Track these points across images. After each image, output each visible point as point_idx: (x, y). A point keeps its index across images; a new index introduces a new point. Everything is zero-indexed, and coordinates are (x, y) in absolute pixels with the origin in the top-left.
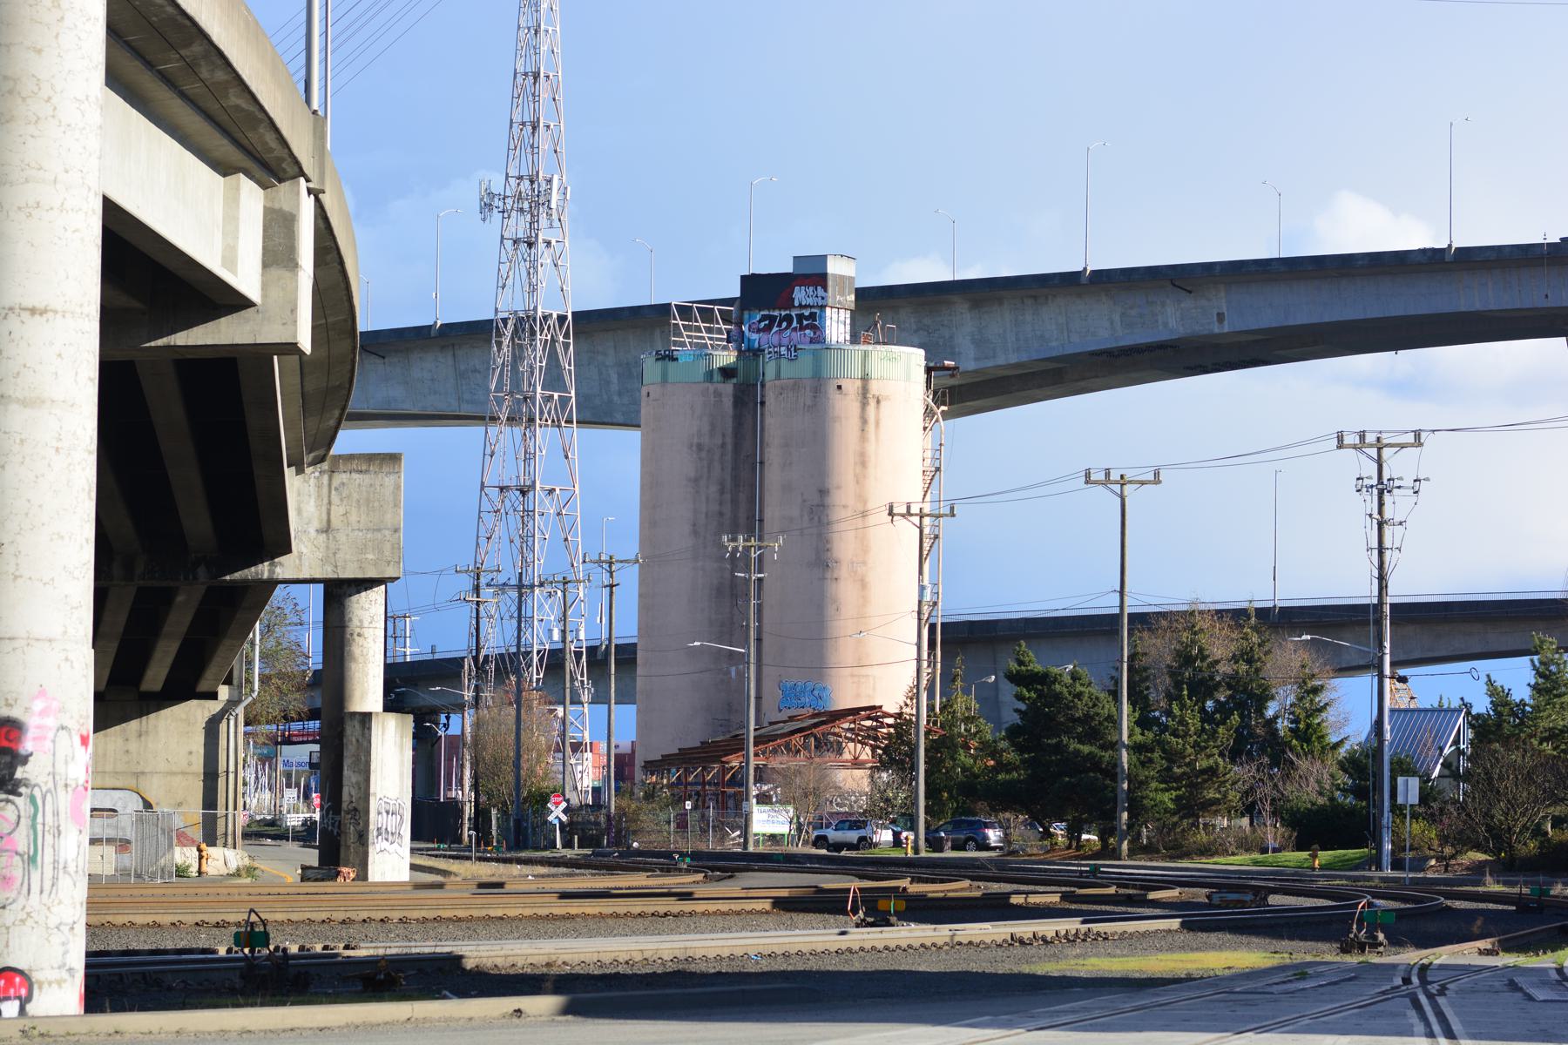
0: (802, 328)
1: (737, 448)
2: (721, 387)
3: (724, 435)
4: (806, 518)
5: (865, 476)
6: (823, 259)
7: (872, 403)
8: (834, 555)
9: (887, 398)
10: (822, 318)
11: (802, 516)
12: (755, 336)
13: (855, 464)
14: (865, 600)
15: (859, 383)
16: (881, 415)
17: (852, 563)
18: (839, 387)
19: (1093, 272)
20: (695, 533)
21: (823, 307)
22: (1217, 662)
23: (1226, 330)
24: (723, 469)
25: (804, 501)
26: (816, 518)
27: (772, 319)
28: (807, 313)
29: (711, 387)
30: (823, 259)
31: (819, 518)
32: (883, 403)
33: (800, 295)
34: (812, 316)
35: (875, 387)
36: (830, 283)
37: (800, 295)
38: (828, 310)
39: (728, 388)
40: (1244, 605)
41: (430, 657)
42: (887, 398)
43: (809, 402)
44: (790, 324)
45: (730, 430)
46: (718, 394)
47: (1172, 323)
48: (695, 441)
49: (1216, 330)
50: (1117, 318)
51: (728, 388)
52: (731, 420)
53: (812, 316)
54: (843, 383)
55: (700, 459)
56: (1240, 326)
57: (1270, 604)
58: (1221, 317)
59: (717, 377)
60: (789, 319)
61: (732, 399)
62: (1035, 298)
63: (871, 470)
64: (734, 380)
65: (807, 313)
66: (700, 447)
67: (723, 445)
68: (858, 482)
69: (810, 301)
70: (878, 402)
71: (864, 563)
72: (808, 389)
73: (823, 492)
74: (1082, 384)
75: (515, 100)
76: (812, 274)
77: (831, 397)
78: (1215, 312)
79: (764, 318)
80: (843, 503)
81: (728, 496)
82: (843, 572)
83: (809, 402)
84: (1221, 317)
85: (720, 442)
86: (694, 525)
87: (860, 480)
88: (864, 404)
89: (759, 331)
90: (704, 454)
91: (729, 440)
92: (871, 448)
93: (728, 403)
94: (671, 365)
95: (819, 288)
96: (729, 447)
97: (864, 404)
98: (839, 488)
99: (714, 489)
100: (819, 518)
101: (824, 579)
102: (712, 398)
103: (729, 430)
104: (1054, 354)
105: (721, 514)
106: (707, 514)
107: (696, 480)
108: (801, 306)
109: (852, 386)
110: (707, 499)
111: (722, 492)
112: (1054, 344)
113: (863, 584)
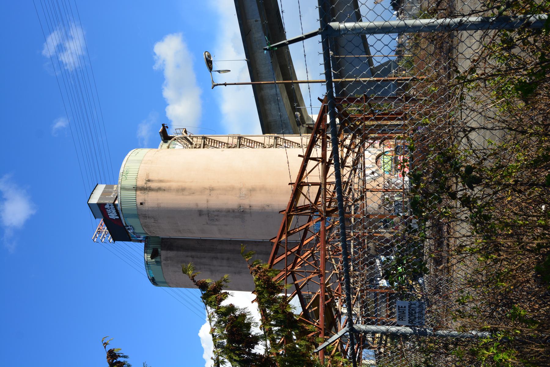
1: (193, 249)
2: (163, 257)
3: (187, 256)
4: (217, 223)
5: (190, 189)
7: (150, 184)
8: (237, 208)
9: (148, 175)
11: (216, 225)
13: (183, 195)
14: (263, 189)
15: (138, 193)
16: (157, 179)
17: (240, 197)
18: (141, 204)
19: (246, 58)
20: (239, 273)
22: (459, 137)
23: (260, 19)
24: (205, 258)
25: (207, 223)
26: (216, 217)
29: (163, 262)
31: (215, 216)
32: (150, 178)
35: (141, 183)
36: (102, 202)
39: (163, 253)
42: (148, 175)
43: (152, 220)
45: (184, 253)
46: (166, 259)
49: (260, 22)
51: (163, 253)
52: (179, 252)
54: (139, 201)
55: (200, 269)
56: (258, 15)
58: (256, 21)
59: (158, 259)
61: (168, 252)
62: (258, 74)
63: (187, 185)
64: (159, 250)
67: (192, 257)
68: (193, 193)
69: (114, 211)
70: (149, 181)
71: (240, 189)
72: (146, 221)
73: (200, 213)
74: (287, 60)
77: (147, 208)
78: (255, 23)
80: (206, 202)
81: (219, 255)
82: (246, 202)
83: (152, 220)
84: (256, 21)
85: (191, 258)
86: (235, 273)
87: (192, 192)
88: (149, 189)
91: (190, 253)
92: (174, 185)
93: (171, 254)
95: (106, 207)
96: (193, 253)
97: (149, 189)
98: (197, 205)
99: (215, 262)
100: (215, 216)
101: (250, 213)
102: (169, 262)
105: (228, 259)
106: (229, 267)
109: (141, 197)
110: (221, 266)
111: (216, 258)
112: (270, 68)
113: (252, 190)
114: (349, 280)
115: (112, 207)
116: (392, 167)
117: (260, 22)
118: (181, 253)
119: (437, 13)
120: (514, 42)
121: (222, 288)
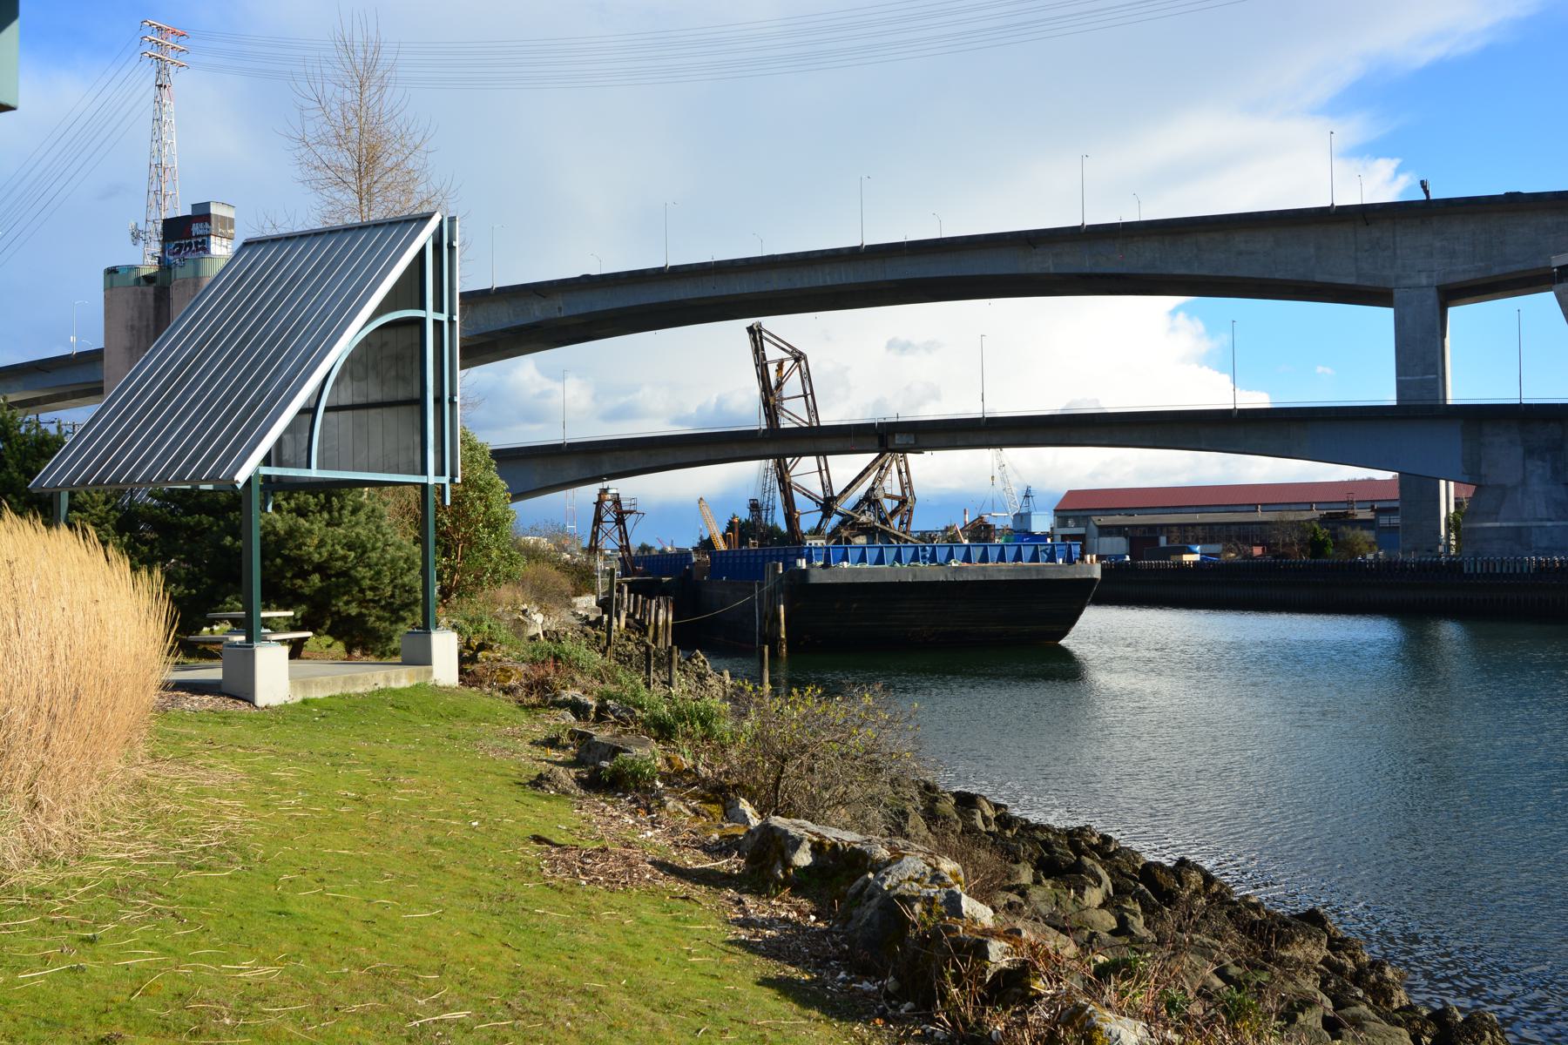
0: (198, 250)
2: (145, 288)
3: (148, 320)
6: (207, 204)
10: (209, 242)
12: (171, 258)
19: (497, 288)
21: (209, 236)
27: (180, 246)
28: (200, 240)
29: (139, 289)
30: (207, 204)
33: (196, 229)
34: (203, 242)
36: (213, 219)
37: (196, 229)
38: (212, 238)
39: (150, 290)
40: (873, 422)
41: (895, 420)
44: (191, 248)
46: (143, 293)
47: (537, 313)
48: (130, 324)
50: (511, 312)
51: (150, 290)
53: (203, 242)
55: (133, 335)
56: (570, 313)
57: (758, 428)
58: (560, 309)
59: (142, 282)
60: (190, 245)
65: (200, 240)
66: (132, 327)
67: (148, 326)
69: (201, 232)
75: (767, 494)
76: (202, 214)
79: (176, 246)
84: (560, 309)
89: (174, 254)
90: (135, 332)
93: (150, 299)
94: (115, 276)
96: (152, 327)
103: (152, 317)
104: (484, 331)
107: (130, 349)
108: (197, 236)
114: (208, 514)
115: (207, 232)
116: (1082, 946)
117: (558, 315)
118: (152, 311)
119: (217, 519)
120: (876, 1017)
121: (292, 622)
